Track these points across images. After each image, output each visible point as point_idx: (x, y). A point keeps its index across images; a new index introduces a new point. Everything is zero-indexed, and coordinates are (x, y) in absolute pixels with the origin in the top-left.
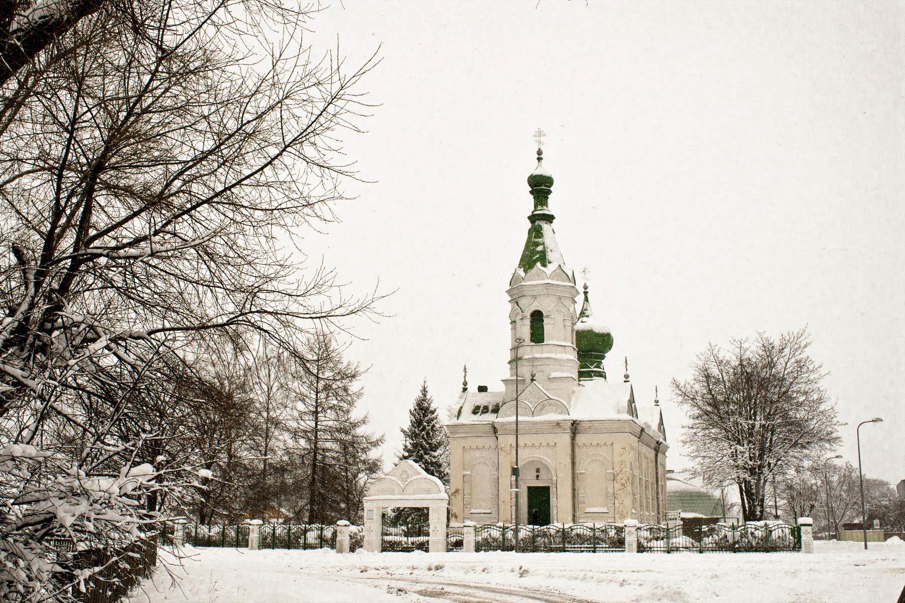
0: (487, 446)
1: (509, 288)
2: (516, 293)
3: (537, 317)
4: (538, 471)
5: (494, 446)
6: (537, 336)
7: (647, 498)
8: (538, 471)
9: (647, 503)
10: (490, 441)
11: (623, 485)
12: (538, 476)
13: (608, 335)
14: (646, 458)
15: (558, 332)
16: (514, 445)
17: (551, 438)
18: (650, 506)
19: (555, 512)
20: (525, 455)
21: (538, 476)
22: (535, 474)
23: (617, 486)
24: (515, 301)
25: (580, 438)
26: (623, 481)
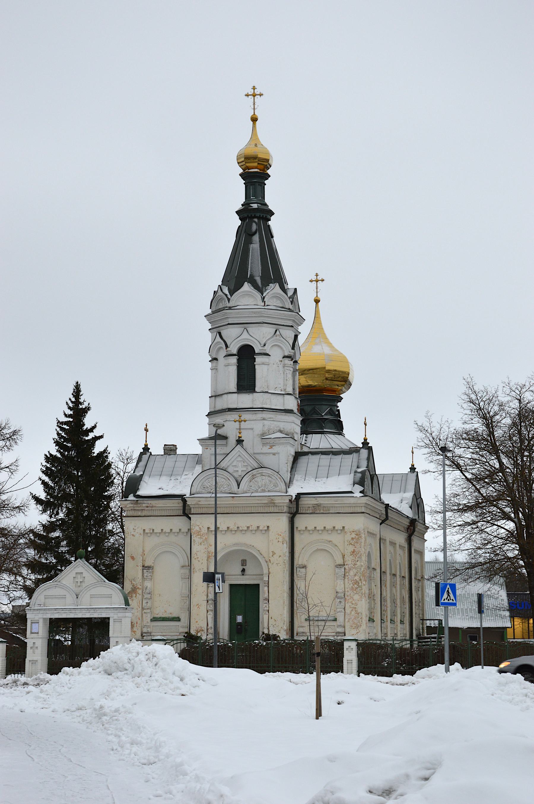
0: (175, 530)
1: (209, 311)
2: (219, 312)
3: (246, 356)
4: (244, 562)
5: (185, 530)
6: (246, 382)
7: (394, 602)
8: (244, 562)
9: (394, 614)
10: (179, 523)
11: (356, 582)
12: (243, 570)
13: (351, 385)
14: (393, 544)
15: (273, 375)
16: (213, 528)
17: (261, 521)
18: (398, 618)
19: (266, 617)
20: (226, 542)
21: (243, 570)
22: (241, 568)
23: (349, 585)
24: (217, 331)
25: (301, 522)
26: (357, 578)
